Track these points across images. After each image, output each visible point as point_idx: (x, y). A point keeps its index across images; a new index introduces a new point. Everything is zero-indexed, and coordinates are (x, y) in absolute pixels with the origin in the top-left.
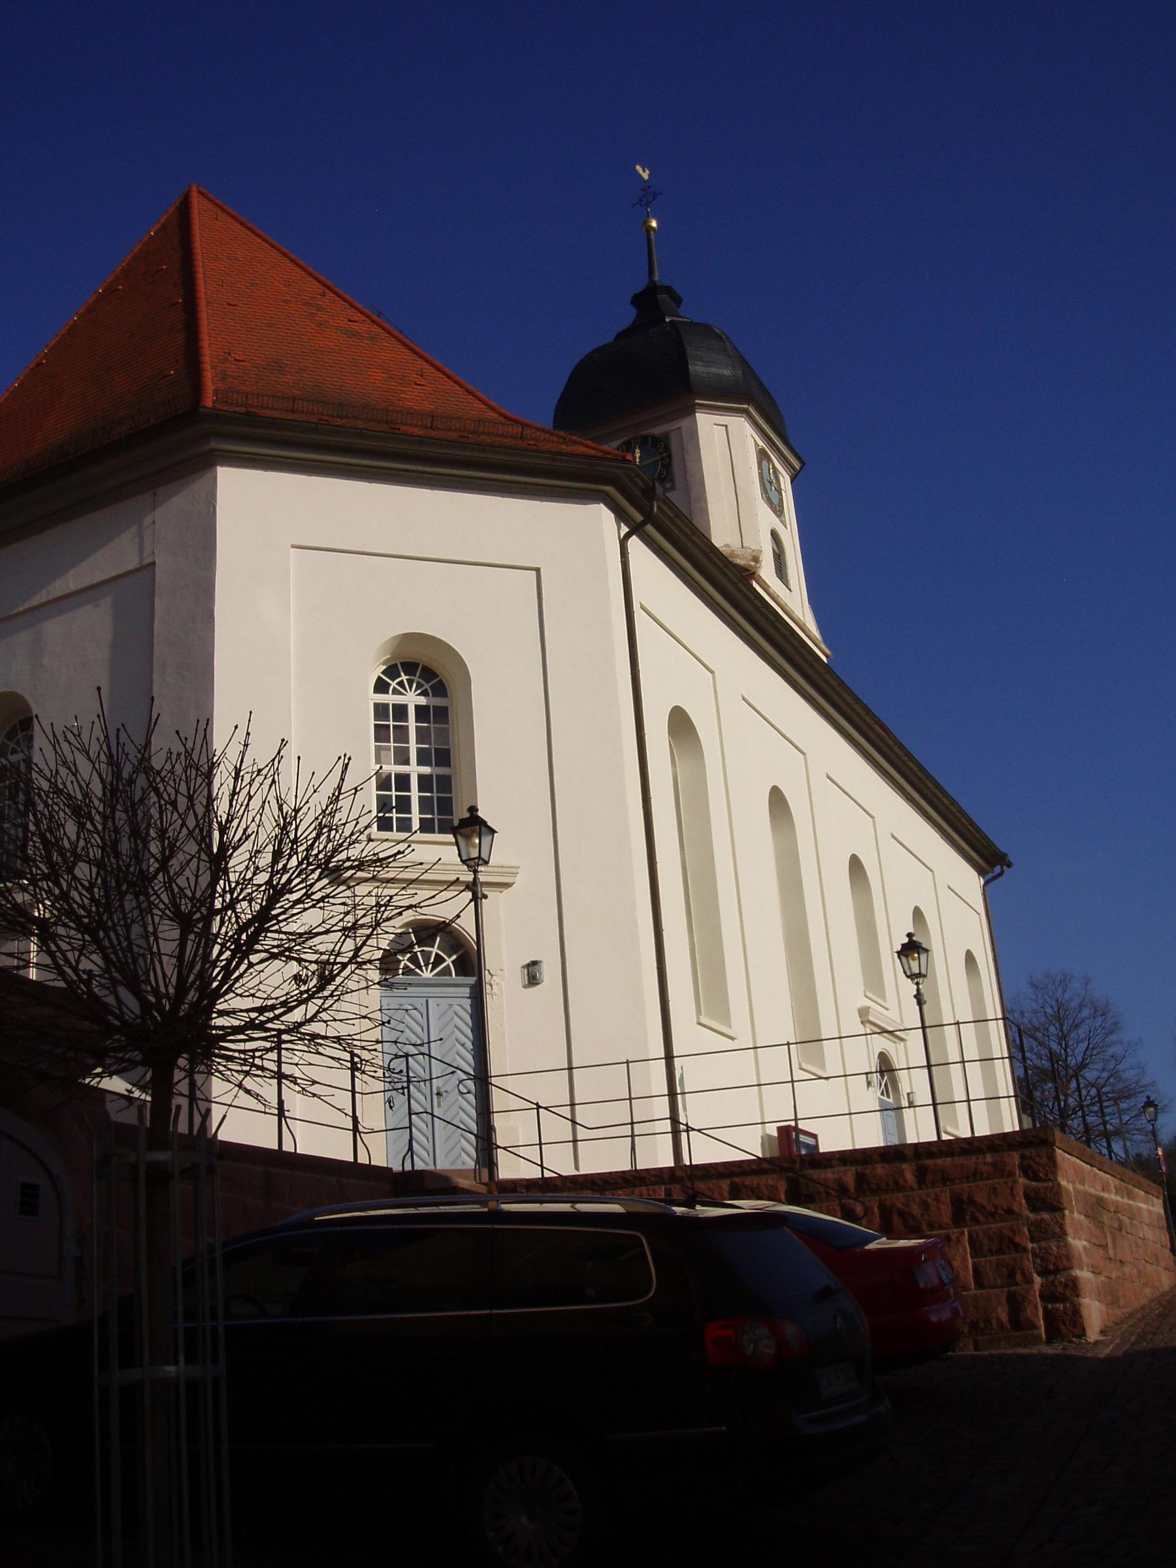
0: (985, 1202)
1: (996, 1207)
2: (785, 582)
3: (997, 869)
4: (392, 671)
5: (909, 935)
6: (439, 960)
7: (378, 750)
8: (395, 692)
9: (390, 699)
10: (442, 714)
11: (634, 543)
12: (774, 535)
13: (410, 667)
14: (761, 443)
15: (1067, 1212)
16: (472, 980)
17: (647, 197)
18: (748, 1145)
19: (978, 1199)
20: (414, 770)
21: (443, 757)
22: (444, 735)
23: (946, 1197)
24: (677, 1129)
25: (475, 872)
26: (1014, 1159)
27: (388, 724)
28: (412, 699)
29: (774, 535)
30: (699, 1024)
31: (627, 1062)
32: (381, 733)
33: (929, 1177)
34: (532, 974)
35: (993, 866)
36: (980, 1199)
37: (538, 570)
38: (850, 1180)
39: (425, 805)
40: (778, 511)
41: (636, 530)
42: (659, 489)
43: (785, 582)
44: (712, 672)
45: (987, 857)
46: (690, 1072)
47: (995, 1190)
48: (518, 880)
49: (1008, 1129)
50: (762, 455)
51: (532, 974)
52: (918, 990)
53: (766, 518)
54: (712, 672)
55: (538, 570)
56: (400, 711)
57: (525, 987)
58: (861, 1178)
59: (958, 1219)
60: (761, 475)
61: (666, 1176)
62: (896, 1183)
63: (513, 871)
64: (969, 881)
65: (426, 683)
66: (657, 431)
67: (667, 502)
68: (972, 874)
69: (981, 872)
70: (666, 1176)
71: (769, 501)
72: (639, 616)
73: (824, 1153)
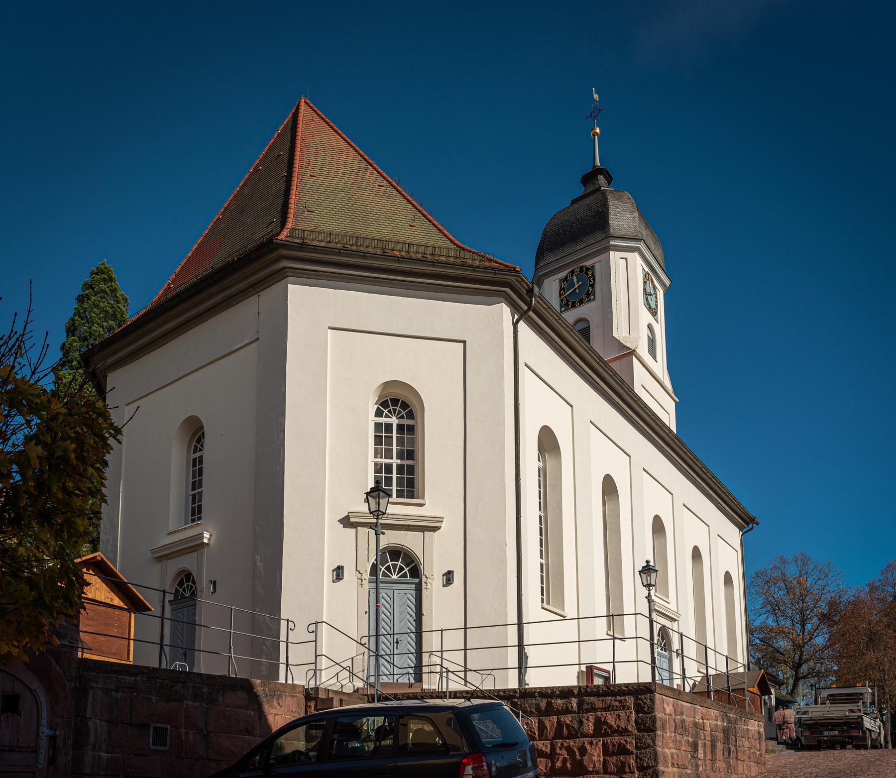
0: (613, 723)
1: (618, 726)
2: (654, 357)
3: (750, 526)
4: (384, 404)
5: (648, 562)
6: (401, 569)
7: (376, 449)
8: (387, 416)
9: (383, 420)
10: (411, 429)
11: (522, 325)
12: (650, 327)
13: (395, 402)
14: (647, 269)
15: (658, 733)
16: (417, 580)
17: (595, 114)
18: (569, 679)
19: (610, 722)
20: (395, 462)
21: (411, 455)
22: (412, 442)
23: (592, 719)
24: (522, 667)
25: (378, 519)
26: (630, 700)
27: (382, 434)
28: (394, 421)
29: (650, 327)
30: (543, 608)
31: (442, 630)
32: (378, 440)
33: (585, 707)
34: (449, 577)
35: (748, 524)
36: (611, 721)
37: (464, 342)
38: (543, 704)
39: (400, 483)
40: (654, 313)
41: (523, 315)
42: (536, 289)
43: (654, 357)
44: (572, 406)
45: (744, 521)
46: (531, 634)
47: (619, 716)
48: (443, 525)
49: (511, 686)
50: (646, 277)
51: (449, 577)
52: (649, 594)
53: (645, 317)
54: (572, 406)
55: (464, 342)
56: (389, 427)
57: (444, 586)
58: (549, 704)
59: (597, 733)
60: (645, 290)
61: (576, 692)
62: (567, 708)
63: (440, 520)
64: (733, 534)
65: (400, 408)
66: (588, 263)
67: (541, 297)
68: (736, 530)
69: (740, 528)
70: (576, 692)
71: (649, 308)
72: (522, 368)
73: (620, 685)
